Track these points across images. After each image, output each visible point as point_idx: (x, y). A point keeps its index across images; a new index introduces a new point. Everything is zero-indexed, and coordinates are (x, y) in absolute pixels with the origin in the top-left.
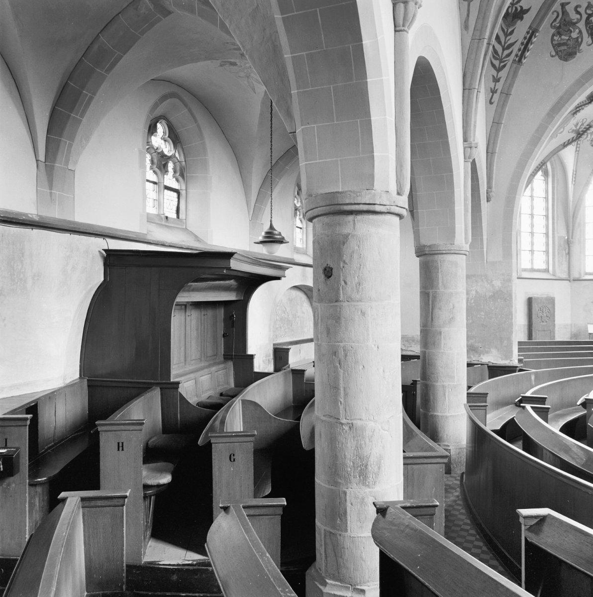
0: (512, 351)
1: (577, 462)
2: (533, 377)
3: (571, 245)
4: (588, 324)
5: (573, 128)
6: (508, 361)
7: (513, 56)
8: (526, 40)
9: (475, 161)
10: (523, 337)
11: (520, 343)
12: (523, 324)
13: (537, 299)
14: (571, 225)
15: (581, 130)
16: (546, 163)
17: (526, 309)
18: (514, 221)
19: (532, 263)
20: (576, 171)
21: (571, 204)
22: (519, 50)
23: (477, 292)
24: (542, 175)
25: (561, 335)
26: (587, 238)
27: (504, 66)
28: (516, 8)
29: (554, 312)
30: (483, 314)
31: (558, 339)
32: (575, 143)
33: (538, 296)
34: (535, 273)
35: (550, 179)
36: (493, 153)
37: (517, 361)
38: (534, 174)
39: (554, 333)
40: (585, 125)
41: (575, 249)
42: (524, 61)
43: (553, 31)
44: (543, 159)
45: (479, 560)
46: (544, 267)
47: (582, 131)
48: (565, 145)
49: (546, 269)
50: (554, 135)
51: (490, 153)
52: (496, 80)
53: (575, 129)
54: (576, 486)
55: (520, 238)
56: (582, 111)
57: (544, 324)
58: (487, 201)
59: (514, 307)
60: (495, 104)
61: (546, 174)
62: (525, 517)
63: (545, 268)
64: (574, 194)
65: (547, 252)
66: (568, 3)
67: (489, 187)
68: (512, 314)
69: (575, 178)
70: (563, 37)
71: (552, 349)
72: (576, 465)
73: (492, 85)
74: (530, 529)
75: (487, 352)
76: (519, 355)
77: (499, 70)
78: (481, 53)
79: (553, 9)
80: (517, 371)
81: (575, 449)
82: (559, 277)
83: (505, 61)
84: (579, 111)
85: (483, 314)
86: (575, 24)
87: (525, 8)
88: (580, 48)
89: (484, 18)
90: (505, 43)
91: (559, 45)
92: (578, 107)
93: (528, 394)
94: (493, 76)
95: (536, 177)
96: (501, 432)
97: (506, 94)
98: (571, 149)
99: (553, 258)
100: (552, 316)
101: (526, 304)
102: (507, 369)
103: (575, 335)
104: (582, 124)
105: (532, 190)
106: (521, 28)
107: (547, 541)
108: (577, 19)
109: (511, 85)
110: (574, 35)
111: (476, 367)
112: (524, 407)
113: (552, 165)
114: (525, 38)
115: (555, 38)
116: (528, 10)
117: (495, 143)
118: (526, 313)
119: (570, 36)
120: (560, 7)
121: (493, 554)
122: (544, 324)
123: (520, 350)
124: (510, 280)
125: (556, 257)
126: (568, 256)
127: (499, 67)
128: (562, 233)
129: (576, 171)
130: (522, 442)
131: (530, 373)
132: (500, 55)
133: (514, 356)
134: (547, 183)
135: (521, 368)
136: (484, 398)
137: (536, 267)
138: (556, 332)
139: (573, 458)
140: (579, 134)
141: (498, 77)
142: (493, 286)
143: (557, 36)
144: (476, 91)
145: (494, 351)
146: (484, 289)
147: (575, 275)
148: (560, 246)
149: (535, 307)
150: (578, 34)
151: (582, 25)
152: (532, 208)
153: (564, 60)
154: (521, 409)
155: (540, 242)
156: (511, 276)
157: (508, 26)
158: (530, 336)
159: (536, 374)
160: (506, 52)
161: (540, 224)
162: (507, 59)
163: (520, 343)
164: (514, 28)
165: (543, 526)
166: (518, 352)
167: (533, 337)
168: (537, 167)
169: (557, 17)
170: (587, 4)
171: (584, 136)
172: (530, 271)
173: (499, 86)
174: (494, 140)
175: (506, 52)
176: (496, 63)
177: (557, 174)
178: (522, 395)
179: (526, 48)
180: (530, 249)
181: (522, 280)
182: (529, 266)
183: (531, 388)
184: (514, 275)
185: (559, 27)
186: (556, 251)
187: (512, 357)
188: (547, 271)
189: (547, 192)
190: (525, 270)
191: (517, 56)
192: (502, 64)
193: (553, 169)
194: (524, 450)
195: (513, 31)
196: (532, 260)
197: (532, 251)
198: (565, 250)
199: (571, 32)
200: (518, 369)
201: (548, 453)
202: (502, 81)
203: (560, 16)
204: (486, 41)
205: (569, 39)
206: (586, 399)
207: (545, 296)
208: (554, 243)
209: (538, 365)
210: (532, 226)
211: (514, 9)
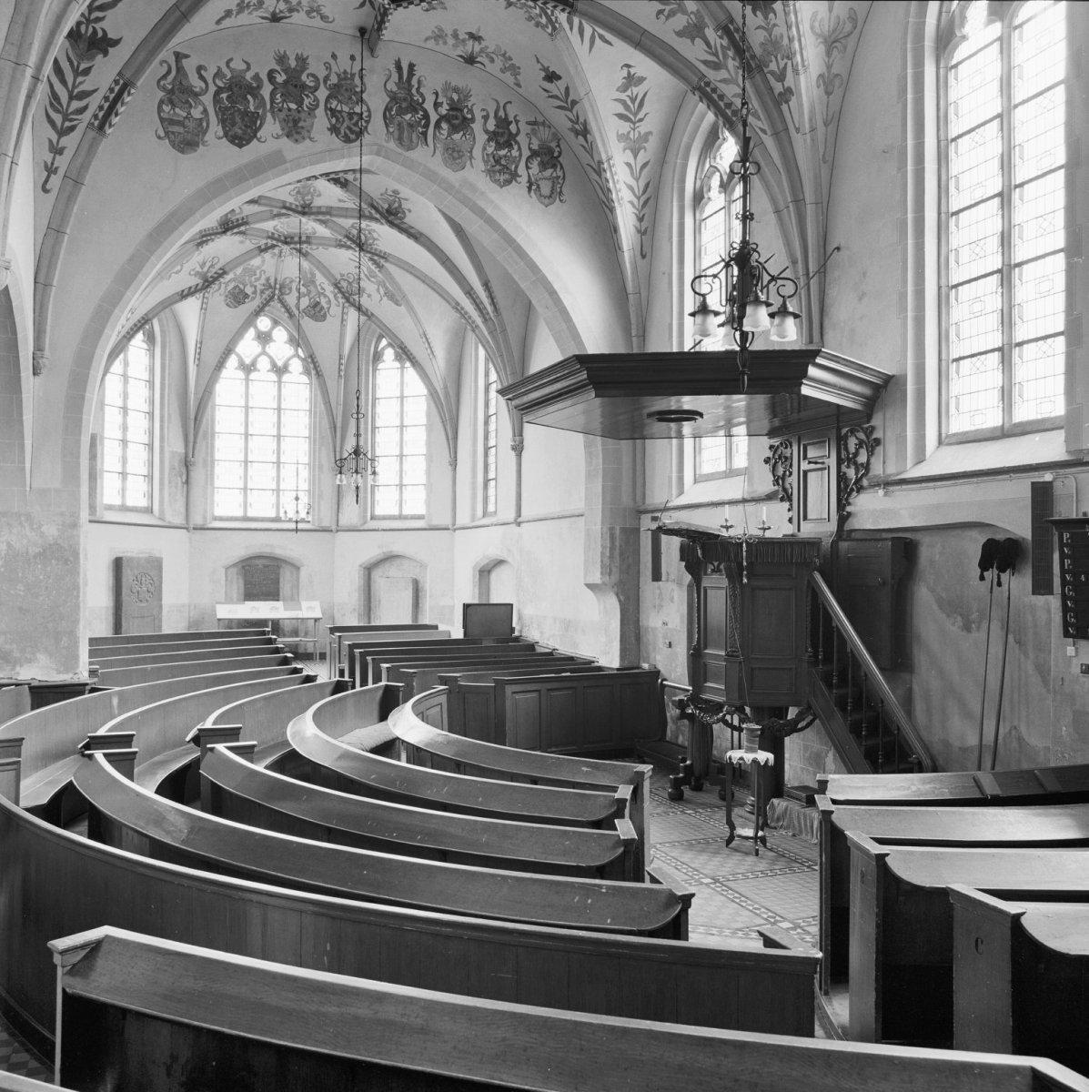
0: (78, 656)
1: (173, 838)
2: (115, 701)
3: (191, 468)
4: (217, 603)
5: (197, 269)
6: (71, 675)
7: (87, 116)
8: (113, 95)
9: (8, 291)
10: (103, 629)
11: (92, 641)
13: (131, 559)
14: (191, 438)
15: (210, 275)
16: (150, 320)
17: (111, 578)
18: (84, 417)
19: (123, 496)
20: (201, 343)
21: (192, 397)
22: (101, 108)
23: (9, 545)
24: (143, 341)
25: (172, 624)
26: (217, 458)
27: (72, 129)
28: (95, 31)
29: (161, 583)
30: (22, 588)
31: (166, 630)
32: (199, 295)
33: (134, 555)
34: (129, 514)
36: (47, 285)
37: (86, 674)
38: (129, 336)
39: (160, 621)
40: (217, 267)
41: (198, 474)
42: (109, 131)
43: (161, 94)
44: (145, 312)
45: (28, 1075)
46: (143, 503)
47: (211, 277)
48: (184, 295)
49: (147, 508)
50: (160, 276)
51: (42, 283)
52: (57, 151)
53: (200, 270)
54: (162, 876)
55: (103, 448)
56: (211, 244)
57: (143, 605)
58: (34, 374)
59: (82, 576)
60: (52, 196)
61: (151, 339)
62: (63, 952)
63: (146, 505)
64: (197, 381)
65: (150, 477)
66: (187, 56)
67: (39, 348)
68: (79, 588)
69: (199, 354)
70: (177, 110)
71: (153, 649)
72: (177, 845)
73: (48, 157)
74: (74, 971)
75: (29, 661)
76: (91, 663)
77: (62, 132)
78: (19, 92)
79: (161, 57)
80: (87, 692)
81: (171, 817)
82: (169, 522)
83: (75, 120)
84: (207, 241)
85: (22, 588)
86: (196, 95)
87: (111, 35)
88: (206, 139)
89: (25, 25)
90: (74, 86)
91: (172, 122)
92: (203, 236)
93: (102, 732)
94: (50, 141)
95: (133, 342)
96: (47, 811)
97: (75, 181)
98: (192, 304)
99: (161, 490)
100: (157, 592)
101: (111, 568)
102: (65, 690)
103: (196, 623)
104: (212, 266)
105: (126, 364)
106: (104, 72)
107: (101, 987)
108: (201, 88)
109: (84, 167)
110: (197, 113)
111: (6, 691)
112: (90, 757)
113: (161, 326)
114: (111, 90)
115: (164, 107)
116: (116, 43)
117: (51, 266)
118: (111, 585)
119: (189, 113)
120: (174, 58)
121: (18, 1042)
122: (143, 605)
123: (92, 654)
124: (75, 525)
125: (166, 487)
126: (185, 486)
127: (62, 129)
128: (178, 447)
129: (201, 343)
130: (86, 823)
131: (110, 696)
132: (65, 107)
133: (81, 664)
134: (152, 356)
135: (94, 686)
136: (16, 749)
137: (130, 503)
138: (164, 619)
139: (168, 833)
140: (206, 281)
141: (60, 146)
142: (42, 535)
143: (167, 106)
144: (9, 160)
146: (25, 541)
147: (197, 519)
148: (172, 468)
150: (202, 113)
151: (207, 99)
152: (125, 396)
153: (178, 151)
154: (86, 759)
155: (138, 459)
156: (78, 517)
157: (81, 58)
158: (117, 626)
159: (120, 694)
160: (76, 105)
161: (138, 427)
162: (79, 117)
163: (92, 641)
164: (91, 65)
165: (95, 959)
166: (90, 658)
167: (123, 629)
168: (135, 325)
169: (169, 72)
171: (215, 287)
172: (120, 510)
173: (62, 162)
174: (50, 262)
175: (76, 105)
176: (57, 118)
177: (170, 342)
178: (89, 735)
179: (111, 110)
180: (120, 470)
182: (117, 502)
183: (112, 719)
184: (84, 515)
185: (171, 92)
186: (166, 476)
187: (78, 667)
188: (149, 510)
189: (152, 371)
190: (110, 508)
191: (96, 116)
192: (67, 124)
193: (162, 331)
194: (90, 837)
195: (90, 68)
196: (123, 490)
197: (124, 475)
198: (181, 476)
199: (191, 106)
200: (88, 688)
201: (130, 832)
202: (68, 154)
204: (29, 72)
205: (187, 117)
206: (199, 730)
207: (147, 555)
208: (162, 462)
209: (126, 679)
210: (125, 428)
211: (91, 30)
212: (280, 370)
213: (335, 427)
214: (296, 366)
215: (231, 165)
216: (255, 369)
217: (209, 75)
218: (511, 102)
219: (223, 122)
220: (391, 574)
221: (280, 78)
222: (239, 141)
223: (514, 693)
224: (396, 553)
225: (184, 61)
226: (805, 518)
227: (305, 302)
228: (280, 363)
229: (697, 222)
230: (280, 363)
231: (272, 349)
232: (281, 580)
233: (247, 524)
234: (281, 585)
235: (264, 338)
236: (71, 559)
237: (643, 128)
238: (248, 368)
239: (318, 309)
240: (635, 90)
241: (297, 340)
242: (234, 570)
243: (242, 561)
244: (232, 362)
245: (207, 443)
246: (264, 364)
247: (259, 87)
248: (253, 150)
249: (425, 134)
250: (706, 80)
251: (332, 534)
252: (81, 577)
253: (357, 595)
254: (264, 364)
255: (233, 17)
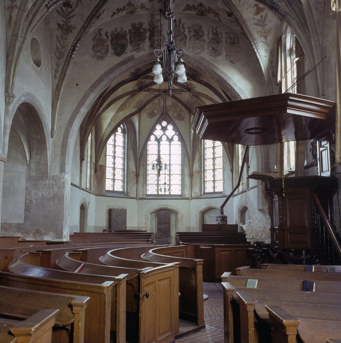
12: (105, 226)
13: (113, 209)
24: (121, 133)
35: (126, 135)
58: (51, 138)
60: (58, 78)
63: (122, 191)
66: (102, 30)
75: (47, 234)
77: (59, 58)
114: (73, 43)
128: (133, 168)
137: (116, 190)
145: (52, 234)
149: (114, 215)
169: (96, 36)
170: (111, 32)
181: (116, 198)
197: (114, 180)
203: (98, 36)
212: (170, 140)
213: (190, 160)
214: (176, 138)
215: (116, 62)
216: (162, 140)
217: (109, 35)
218: (218, 27)
219: (113, 48)
220: (212, 215)
221: (133, 31)
222: (118, 54)
223: (219, 251)
224: (214, 207)
225: (101, 31)
226: (322, 171)
227: (175, 114)
228: (170, 138)
229: (292, 60)
230: (170, 138)
231: (167, 133)
232: (171, 218)
233: (158, 197)
234: (171, 220)
235: (164, 129)
236: (62, 199)
237: (267, 28)
238: (158, 140)
239: (180, 116)
240: (262, 14)
241: (176, 129)
242: (154, 215)
243: (156, 211)
244: (152, 138)
245: (144, 167)
246: (164, 138)
247: (126, 36)
248: (124, 57)
249: (185, 43)
250: (274, 2)
251: (189, 200)
252: (65, 205)
253: (199, 223)
254: (164, 138)
255: (116, 14)
